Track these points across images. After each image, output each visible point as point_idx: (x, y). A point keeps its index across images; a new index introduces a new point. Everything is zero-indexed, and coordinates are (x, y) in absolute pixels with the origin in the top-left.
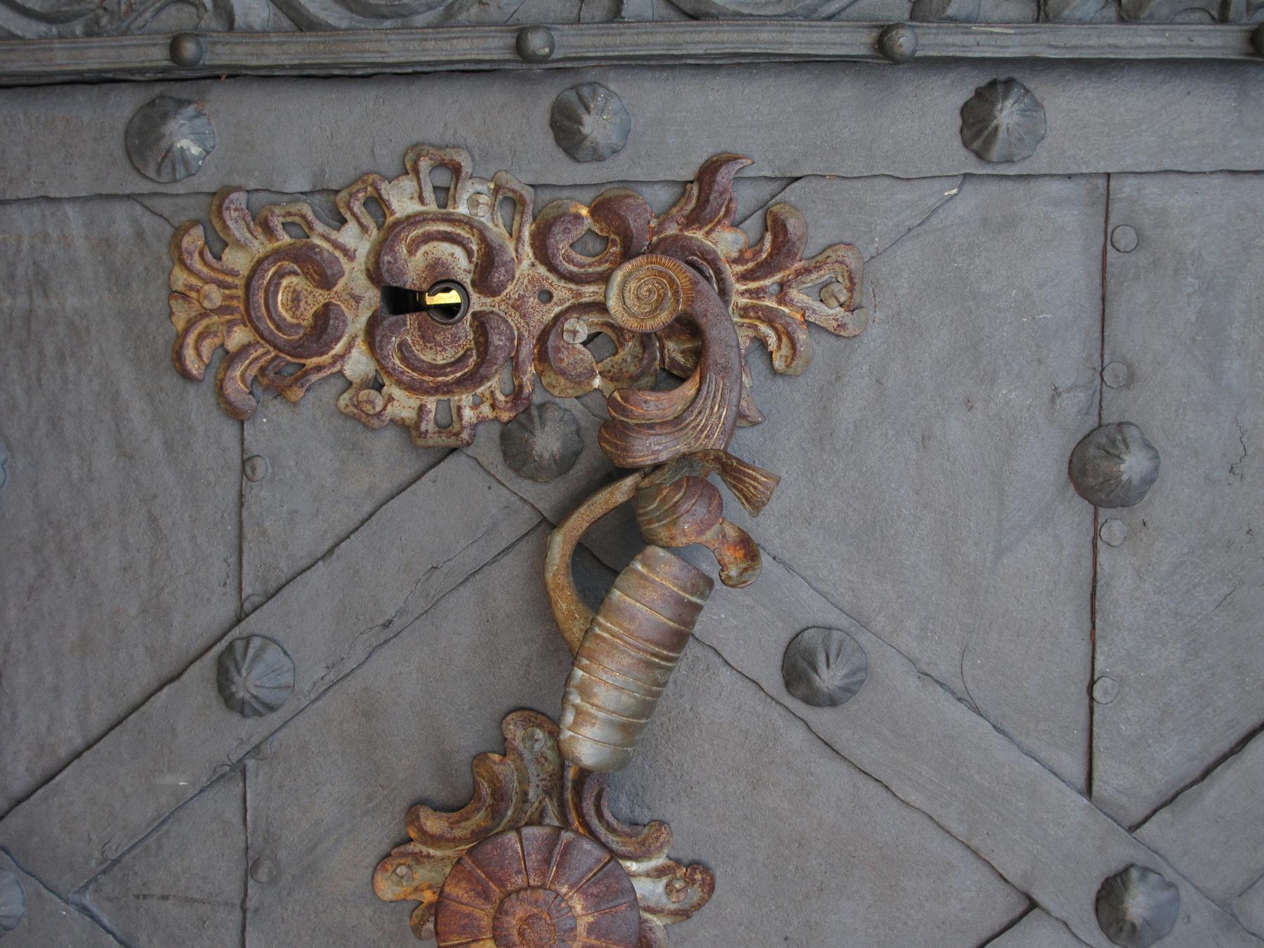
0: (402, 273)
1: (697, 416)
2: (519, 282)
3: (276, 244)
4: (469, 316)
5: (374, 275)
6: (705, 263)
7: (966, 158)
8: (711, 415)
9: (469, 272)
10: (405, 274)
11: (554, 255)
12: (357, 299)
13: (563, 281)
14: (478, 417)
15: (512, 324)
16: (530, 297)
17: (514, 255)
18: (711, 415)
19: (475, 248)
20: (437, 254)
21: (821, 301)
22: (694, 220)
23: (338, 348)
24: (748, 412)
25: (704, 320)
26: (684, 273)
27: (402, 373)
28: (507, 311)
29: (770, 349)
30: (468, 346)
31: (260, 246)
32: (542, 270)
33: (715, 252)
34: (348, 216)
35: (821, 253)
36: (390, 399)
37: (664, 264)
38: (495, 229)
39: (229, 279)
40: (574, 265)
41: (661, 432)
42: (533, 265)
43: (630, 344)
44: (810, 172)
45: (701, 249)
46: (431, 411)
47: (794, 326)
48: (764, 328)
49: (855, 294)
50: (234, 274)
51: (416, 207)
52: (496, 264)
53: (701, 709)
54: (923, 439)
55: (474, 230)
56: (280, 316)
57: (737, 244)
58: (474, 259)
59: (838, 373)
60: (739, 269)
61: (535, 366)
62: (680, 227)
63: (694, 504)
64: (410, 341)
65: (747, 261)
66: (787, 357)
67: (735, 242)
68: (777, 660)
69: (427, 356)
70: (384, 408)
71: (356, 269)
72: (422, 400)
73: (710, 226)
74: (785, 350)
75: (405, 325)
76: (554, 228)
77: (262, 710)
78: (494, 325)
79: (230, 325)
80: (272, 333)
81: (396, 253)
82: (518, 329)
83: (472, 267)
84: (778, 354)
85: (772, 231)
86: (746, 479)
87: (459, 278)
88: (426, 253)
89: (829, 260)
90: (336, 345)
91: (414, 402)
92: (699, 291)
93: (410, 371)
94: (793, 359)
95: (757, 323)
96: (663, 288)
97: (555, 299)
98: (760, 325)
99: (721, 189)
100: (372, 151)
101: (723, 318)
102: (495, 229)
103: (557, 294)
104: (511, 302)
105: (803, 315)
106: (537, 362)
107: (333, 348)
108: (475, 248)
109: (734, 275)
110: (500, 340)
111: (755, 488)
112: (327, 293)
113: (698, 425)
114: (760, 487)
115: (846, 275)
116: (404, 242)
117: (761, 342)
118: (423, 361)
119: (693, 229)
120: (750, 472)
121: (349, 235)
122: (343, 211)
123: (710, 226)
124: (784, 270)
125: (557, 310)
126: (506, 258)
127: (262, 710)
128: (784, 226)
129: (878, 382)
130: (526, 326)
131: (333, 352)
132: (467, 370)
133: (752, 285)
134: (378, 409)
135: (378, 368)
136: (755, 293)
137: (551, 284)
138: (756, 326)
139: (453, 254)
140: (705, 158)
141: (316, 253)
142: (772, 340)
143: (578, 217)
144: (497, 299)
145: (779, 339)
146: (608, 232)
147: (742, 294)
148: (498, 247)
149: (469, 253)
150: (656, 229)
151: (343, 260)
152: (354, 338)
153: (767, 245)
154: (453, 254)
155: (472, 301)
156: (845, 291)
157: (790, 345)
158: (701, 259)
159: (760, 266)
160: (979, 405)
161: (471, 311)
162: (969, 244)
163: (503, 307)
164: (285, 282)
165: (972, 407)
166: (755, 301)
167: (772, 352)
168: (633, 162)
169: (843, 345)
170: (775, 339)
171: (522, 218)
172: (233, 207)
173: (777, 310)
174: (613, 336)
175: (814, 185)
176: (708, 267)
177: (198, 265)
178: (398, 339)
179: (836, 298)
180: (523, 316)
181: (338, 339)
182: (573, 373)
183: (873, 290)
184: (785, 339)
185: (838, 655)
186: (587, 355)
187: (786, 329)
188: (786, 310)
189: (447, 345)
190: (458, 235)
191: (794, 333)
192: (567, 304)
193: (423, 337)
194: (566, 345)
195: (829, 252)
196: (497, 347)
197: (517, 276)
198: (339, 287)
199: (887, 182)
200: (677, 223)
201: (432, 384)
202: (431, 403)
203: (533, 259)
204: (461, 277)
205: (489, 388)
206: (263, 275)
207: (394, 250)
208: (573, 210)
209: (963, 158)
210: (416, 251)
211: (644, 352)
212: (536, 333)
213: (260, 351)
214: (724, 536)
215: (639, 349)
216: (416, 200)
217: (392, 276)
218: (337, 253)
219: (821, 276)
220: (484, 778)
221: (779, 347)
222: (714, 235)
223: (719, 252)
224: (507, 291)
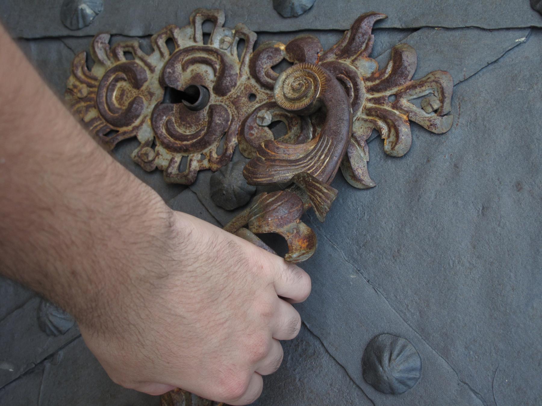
0: (177, 80)
1: (309, 160)
2: (239, 88)
3: (118, 63)
4: (207, 107)
5: (162, 82)
6: (348, 79)
7: (532, 16)
8: (318, 160)
9: (213, 82)
10: (178, 81)
11: (259, 71)
12: (151, 94)
13: (263, 88)
14: (200, 167)
15: (230, 113)
16: (243, 97)
17: (238, 72)
18: (318, 160)
19: (218, 67)
20: (198, 71)
21: (422, 108)
22: (346, 52)
23: (137, 122)
24: (362, 178)
25: (330, 103)
26: (323, 74)
27: (165, 138)
28: (229, 105)
29: (383, 137)
30: (204, 125)
31: (110, 64)
32: (253, 81)
33: (356, 72)
34: (155, 47)
35: (425, 77)
36: (158, 154)
37: (312, 69)
38: (231, 57)
39: (93, 82)
40: (271, 79)
41: (278, 164)
42: (249, 78)
43: (295, 128)
44: (424, 25)
45: (346, 70)
46: (176, 162)
47: (401, 122)
48: (381, 123)
49: (445, 104)
50: (95, 79)
51: (191, 44)
52: (225, 75)
53: (306, 380)
54: (483, 208)
55: (219, 56)
56: (112, 103)
57: (371, 68)
58: (217, 74)
59: (428, 158)
60: (370, 84)
61: (238, 138)
62: (337, 57)
63: (279, 206)
64: (174, 120)
65: (375, 79)
66: (392, 142)
67: (370, 67)
68: (359, 355)
69: (181, 130)
70: (154, 160)
71: (154, 78)
72: (173, 155)
73: (355, 56)
74: (392, 138)
75: (172, 110)
76: (261, 55)
77: (56, 332)
78: (217, 111)
79: (88, 108)
80: (105, 111)
81: (175, 68)
82: (233, 116)
83: (215, 79)
84: (388, 140)
85: (393, 60)
86: (316, 191)
87: (206, 85)
88: (193, 70)
89: (428, 80)
90: (136, 120)
91: (169, 156)
92: (330, 85)
93: (170, 138)
94: (396, 144)
95: (377, 119)
96: (308, 83)
97: (257, 99)
98: (378, 121)
99: (363, 31)
100: (176, 13)
101: (342, 102)
102: (231, 57)
103: (259, 97)
104: (232, 99)
105: (408, 117)
106: (239, 136)
107: (134, 122)
108: (218, 67)
109: (366, 88)
110: (219, 120)
111: (320, 197)
112: (138, 91)
113: (308, 166)
114: (323, 196)
115: (440, 90)
116: (180, 63)
117: (377, 131)
118: (178, 132)
119: (344, 58)
120: (318, 185)
121: (154, 60)
122: (153, 44)
123: (355, 56)
124: (399, 85)
125: (257, 105)
126: (232, 72)
127: (56, 332)
128: (401, 55)
129: (456, 166)
130: (237, 114)
131: (134, 125)
132: (199, 138)
133: (377, 95)
134: (150, 158)
135: (155, 136)
136: (377, 101)
137: (256, 90)
138: (375, 121)
139: (207, 71)
140: (359, 15)
141: (134, 67)
142: (385, 131)
143: (278, 50)
144: (225, 98)
145: (390, 131)
146: (294, 60)
147: (370, 100)
148: (229, 66)
149: (215, 70)
150: (321, 57)
151: (148, 72)
152: (145, 117)
153: (389, 70)
154: (207, 71)
155: (211, 98)
156: (438, 102)
157: (395, 134)
158: (346, 77)
159: (382, 82)
160: (526, 187)
161: (209, 104)
162: (531, 75)
163: (227, 103)
164: (119, 85)
165: (521, 188)
166: (377, 106)
167: (384, 140)
168: (316, 18)
169: (434, 140)
170: (387, 130)
171: (246, 50)
172: (100, 41)
173: (390, 112)
174: (286, 122)
175: (427, 34)
176: (350, 81)
177: (79, 73)
178: (167, 118)
179: (431, 105)
180: (237, 108)
181: (137, 117)
182: (257, 143)
183: (459, 104)
184: (393, 131)
185: (398, 355)
186: (270, 134)
187: (394, 123)
188: (397, 112)
189: (193, 123)
190: (210, 59)
191: (399, 126)
192: (264, 102)
193: (180, 118)
194: (257, 126)
195: (430, 76)
196: (216, 124)
197: (238, 84)
198: (144, 88)
199: (476, 32)
200: (335, 54)
201: (179, 145)
202: (178, 158)
203: (249, 75)
204: (208, 84)
205: (210, 150)
206: (107, 79)
207: (174, 66)
208: (276, 46)
209: (530, 16)
210: (187, 68)
211: (301, 132)
212: (242, 119)
213: (99, 123)
214: (298, 232)
215: (299, 131)
216: (192, 40)
217: (170, 81)
218: (146, 68)
219: (423, 91)
220: (166, 401)
221: (389, 137)
222: (356, 62)
223: (359, 74)
224: (231, 93)
